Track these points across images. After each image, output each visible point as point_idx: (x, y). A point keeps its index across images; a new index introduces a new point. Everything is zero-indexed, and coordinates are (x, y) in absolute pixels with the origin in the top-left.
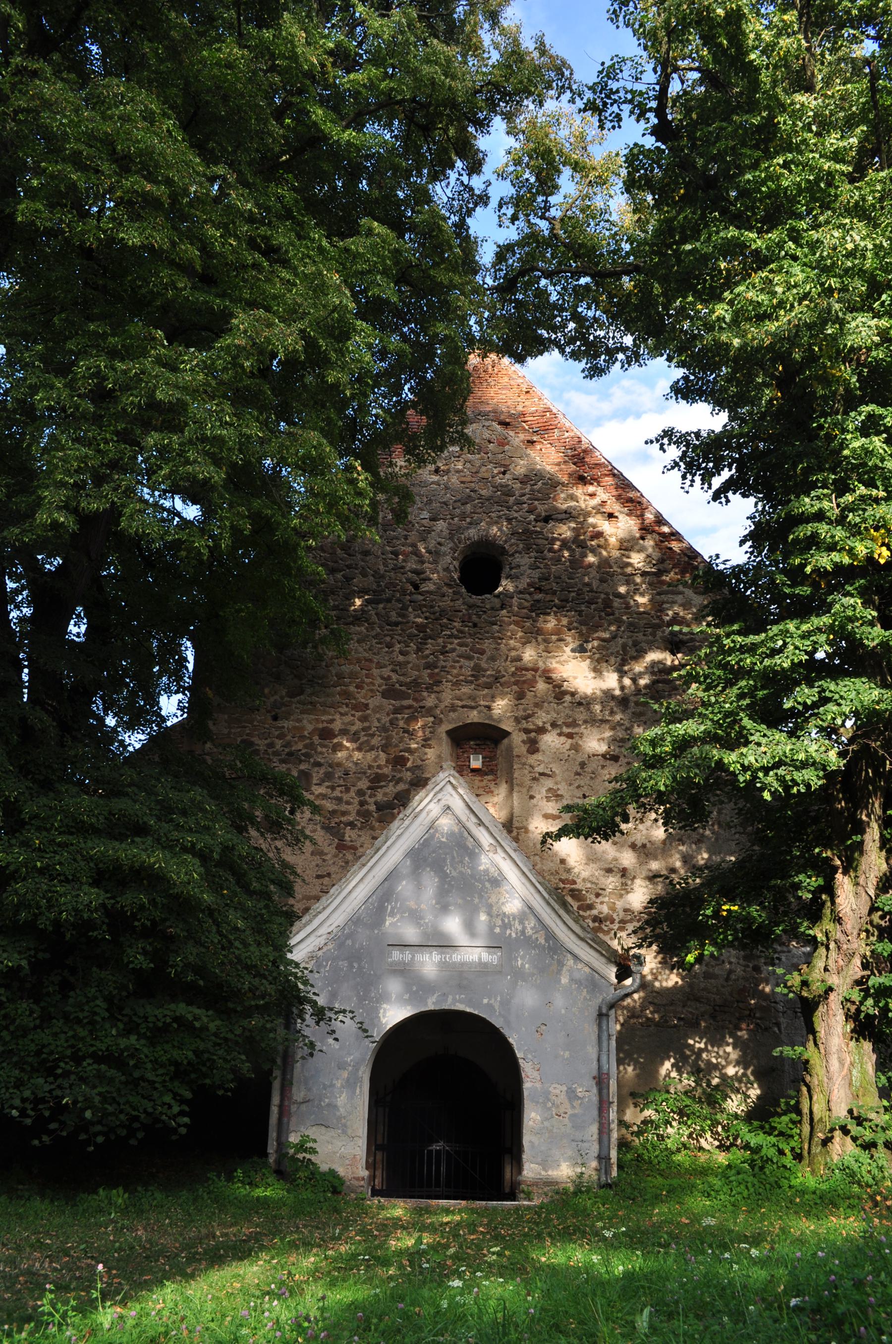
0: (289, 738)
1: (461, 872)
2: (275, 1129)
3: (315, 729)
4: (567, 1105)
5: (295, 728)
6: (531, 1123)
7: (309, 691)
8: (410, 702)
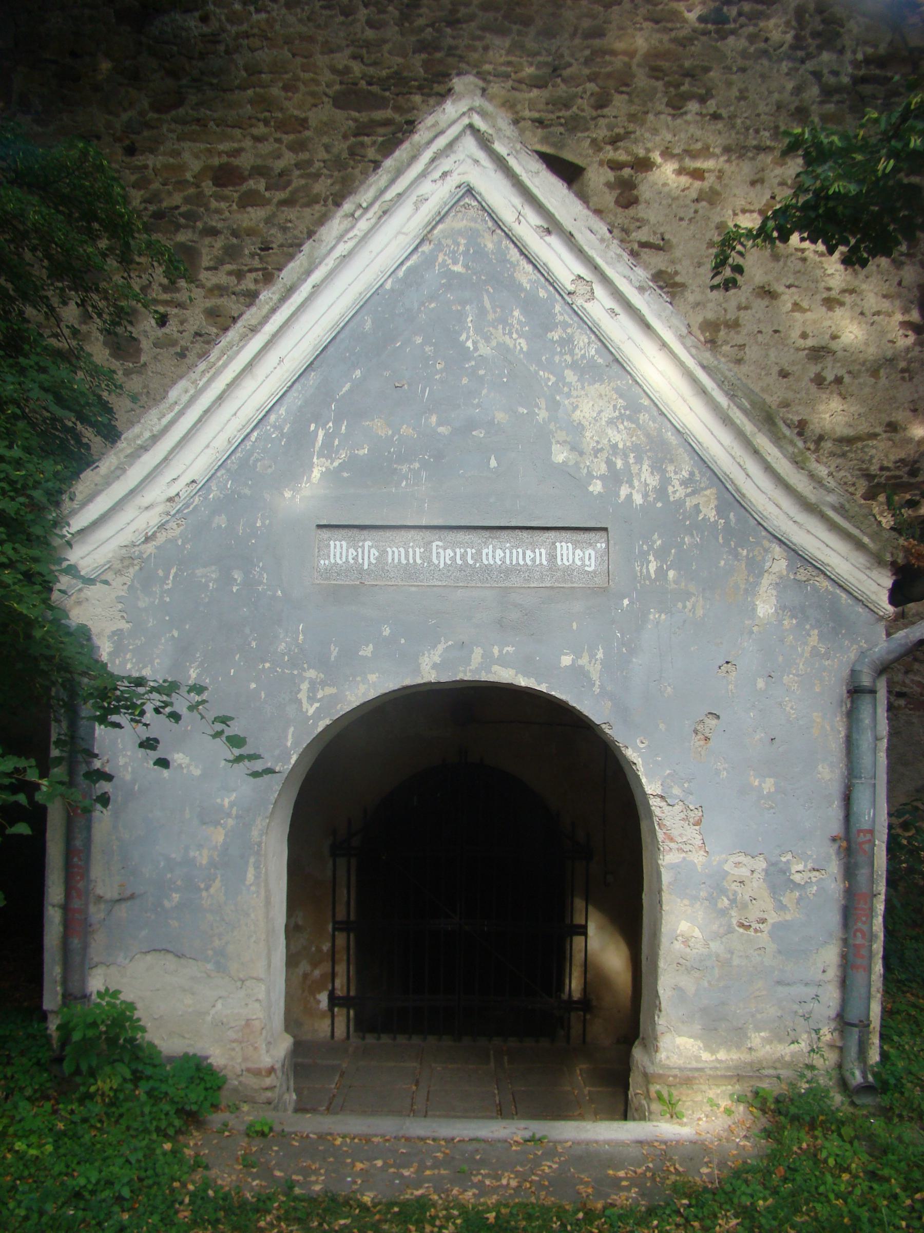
0: (156, 186)
1: (502, 347)
2: (58, 957)
3: (206, 168)
4: (766, 903)
5: (166, 167)
6: (678, 945)
7: (193, 99)
8: (388, 113)
